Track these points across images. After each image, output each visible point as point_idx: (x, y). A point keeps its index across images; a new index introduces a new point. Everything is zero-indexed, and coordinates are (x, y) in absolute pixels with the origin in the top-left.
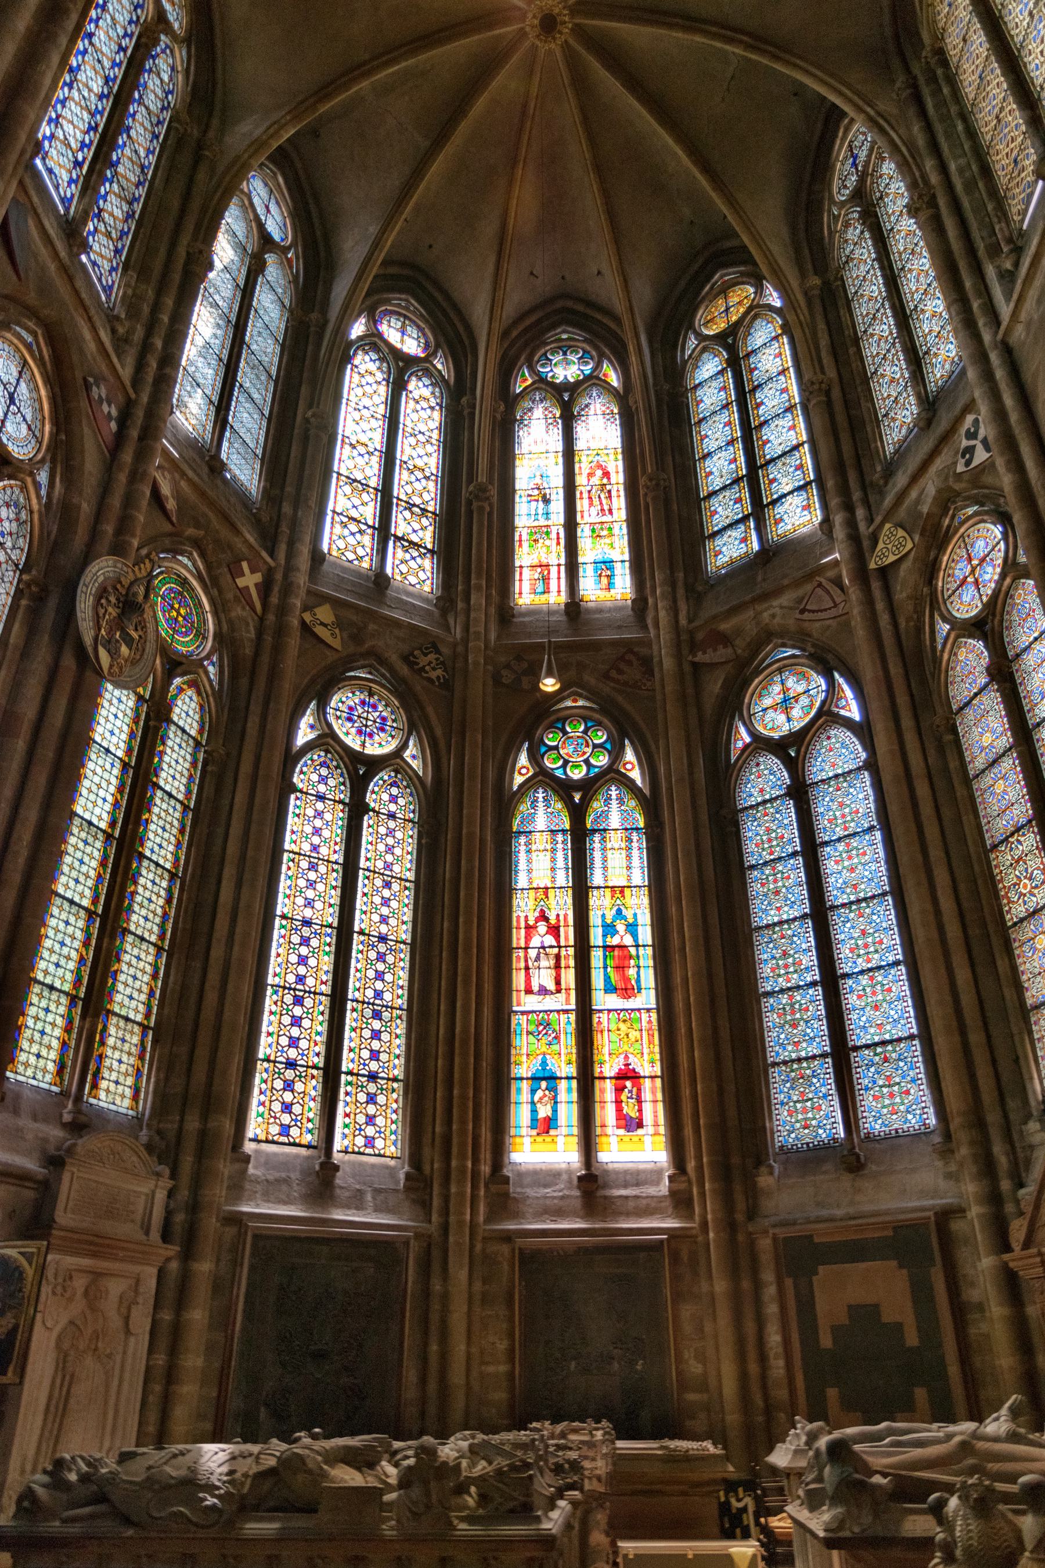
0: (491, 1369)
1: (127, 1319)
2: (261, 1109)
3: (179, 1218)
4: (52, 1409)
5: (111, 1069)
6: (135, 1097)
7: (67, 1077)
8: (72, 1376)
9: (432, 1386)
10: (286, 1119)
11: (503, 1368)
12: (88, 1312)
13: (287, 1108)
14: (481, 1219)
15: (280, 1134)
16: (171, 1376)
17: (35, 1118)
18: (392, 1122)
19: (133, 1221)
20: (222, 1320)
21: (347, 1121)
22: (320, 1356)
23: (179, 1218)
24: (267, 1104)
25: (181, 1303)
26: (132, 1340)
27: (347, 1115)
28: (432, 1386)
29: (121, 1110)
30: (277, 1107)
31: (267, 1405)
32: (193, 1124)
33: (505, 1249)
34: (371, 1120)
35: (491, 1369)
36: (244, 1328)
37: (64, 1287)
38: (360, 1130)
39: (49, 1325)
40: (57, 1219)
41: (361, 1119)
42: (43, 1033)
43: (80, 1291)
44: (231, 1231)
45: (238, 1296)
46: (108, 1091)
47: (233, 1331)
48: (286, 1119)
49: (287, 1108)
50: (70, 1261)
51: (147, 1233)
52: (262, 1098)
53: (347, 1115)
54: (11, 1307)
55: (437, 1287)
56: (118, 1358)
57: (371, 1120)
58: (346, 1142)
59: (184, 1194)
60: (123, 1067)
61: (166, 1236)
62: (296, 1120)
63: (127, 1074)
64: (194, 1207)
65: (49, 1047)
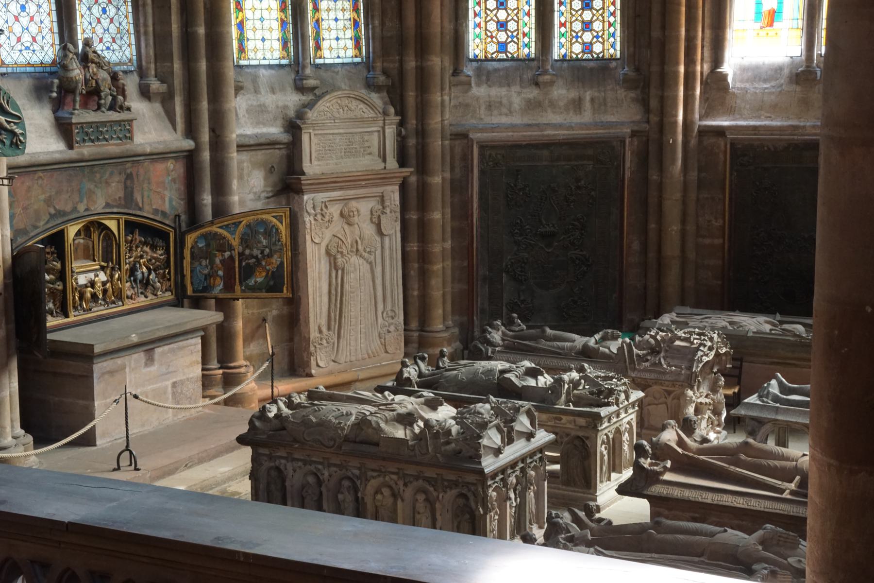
0: (707, 241)
1: (379, 226)
2: (478, 30)
3: (412, 142)
4: (333, 292)
5: (329, 29)
6: (357, 45)
7: (292, 50)
8: (343, 270)
9: (652, 255)
10: (502, 37)
11: (718, 241)
12: (346, 227)
13: (502, 26)
14: (697, 116)
15: (498, 52)
16: (424, 257)
17: (273, 91)
18: (610, 25)
19: (370, 154)
20: (461, 212)
21: (563, 30)
22: (548, 237)
23: (412, 142)
24: (483, 25)
25: (423, 205)
26: (387, 240)
27: (563, 25)
28: (652, 255)
29: (346, 61)
30: (492, 26)
31: (507, 272)
32: (411, 64)
33: (721, 142)
34: (587, 26)
35: (707, 241)
36: (481, 218)
37: (323, 215)
38: (577, 37)
39: (316, 241)
40: (305, 170)
41: (577, 26)
42: (262, 19)
43: (336, 215)
44: (459, 144)
45: (472, 196)
46: (331, 49)
47: (472, 221)
48: (502, 37)
49: (502, 26)
50: (321, 197)
51: (384, 160)
52: (478, 20)
53: (563, 25)
54: (276, 252)
55: (654, 176)
56: (379, 252)
57: (587, 26)
58: (563, 51)
59: (412, 122)
60: (340, 24)
61: (402, 161)
62: (512, 37)
63: (345, 28)
64: (422, 133)
65: (271, 30)
